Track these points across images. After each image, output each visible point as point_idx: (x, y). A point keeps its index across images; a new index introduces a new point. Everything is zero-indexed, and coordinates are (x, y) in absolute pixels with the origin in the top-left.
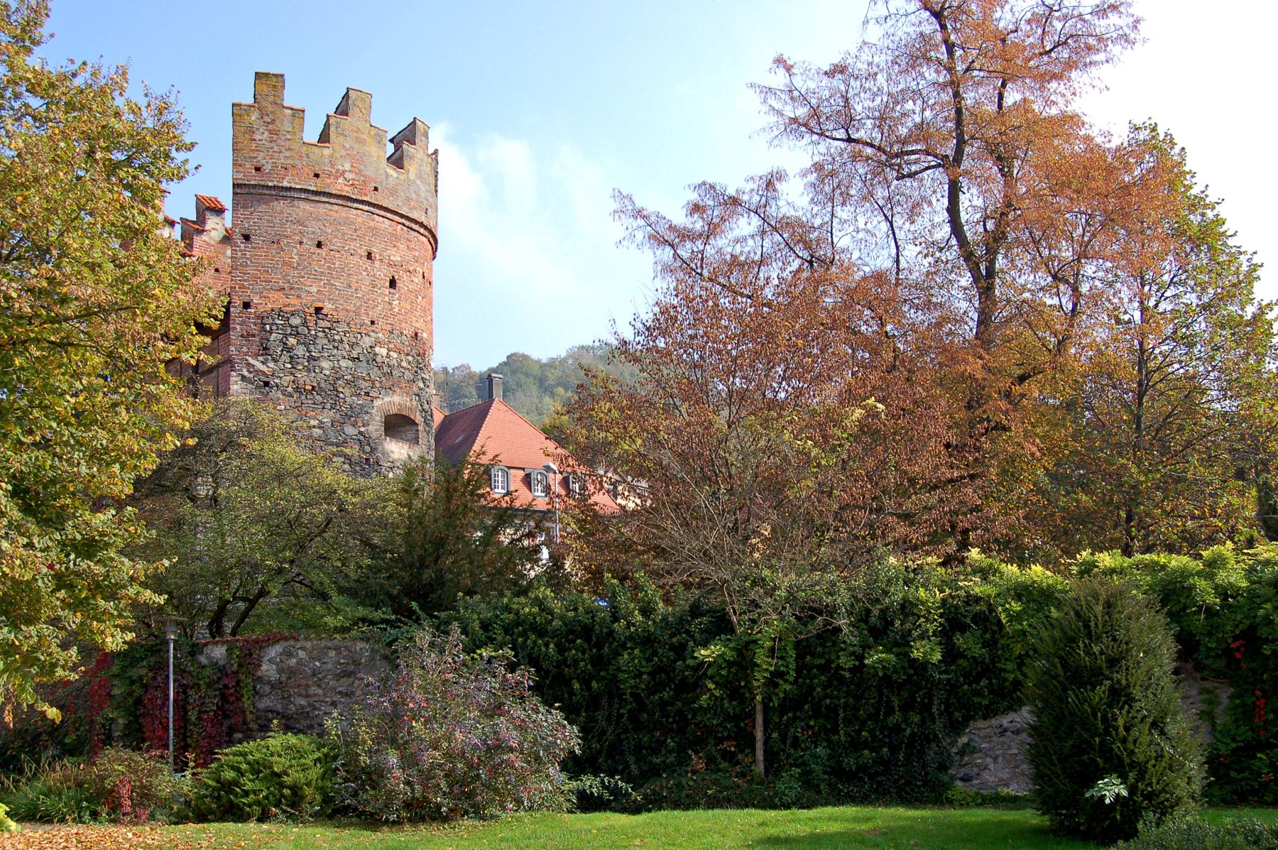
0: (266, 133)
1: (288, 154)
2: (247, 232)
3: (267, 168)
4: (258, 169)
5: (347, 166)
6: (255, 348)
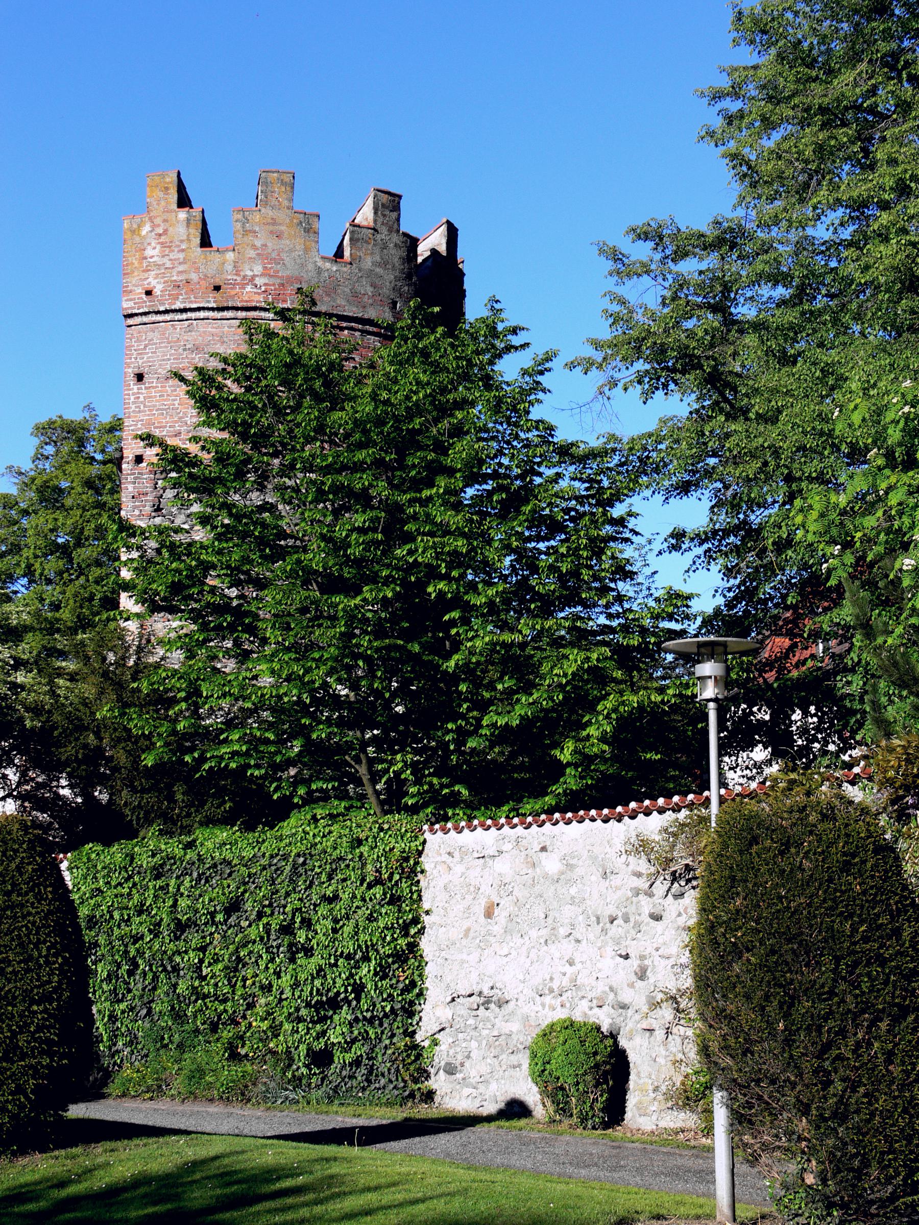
0: (158, 247)
1: (181, 268)
2: (141, 370)
3: (157, 291)
4: (149, 293)
5: (258, 269)
6: (148, 509)
